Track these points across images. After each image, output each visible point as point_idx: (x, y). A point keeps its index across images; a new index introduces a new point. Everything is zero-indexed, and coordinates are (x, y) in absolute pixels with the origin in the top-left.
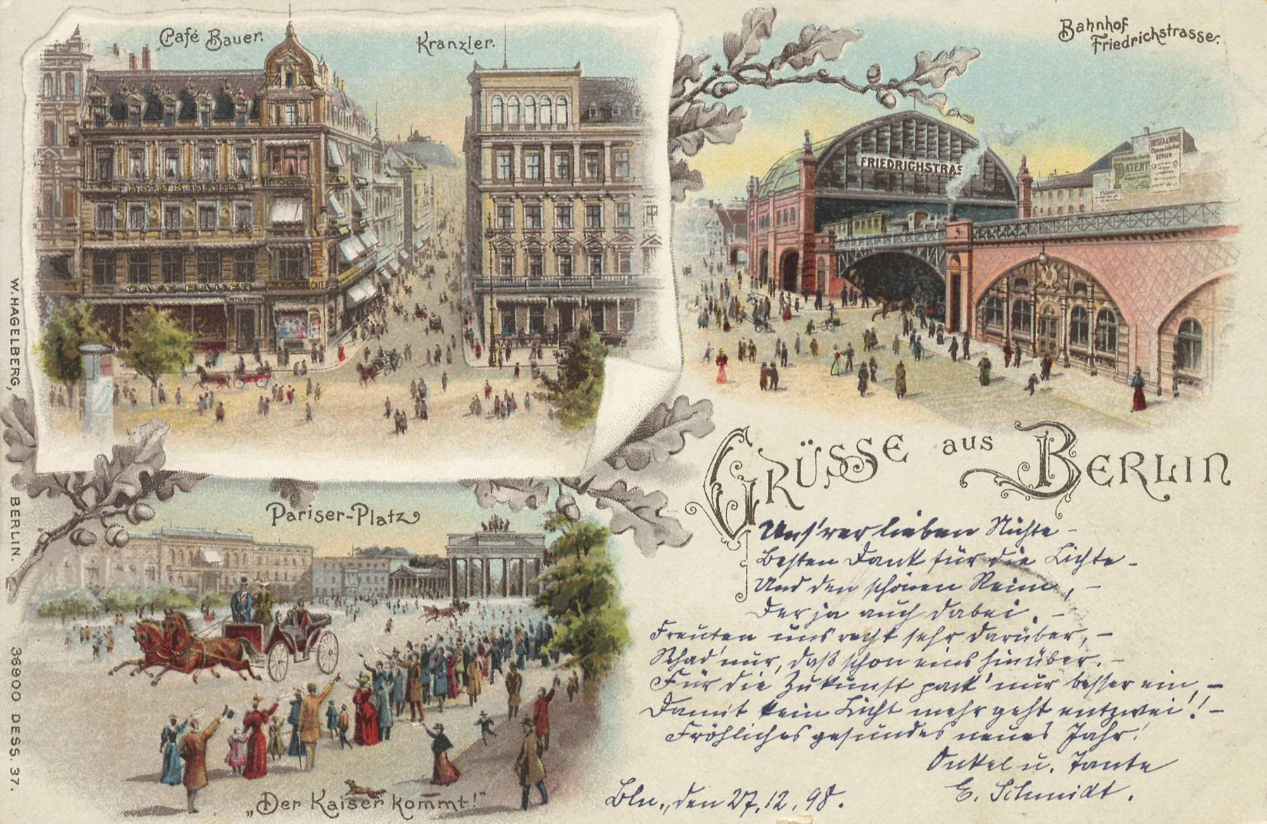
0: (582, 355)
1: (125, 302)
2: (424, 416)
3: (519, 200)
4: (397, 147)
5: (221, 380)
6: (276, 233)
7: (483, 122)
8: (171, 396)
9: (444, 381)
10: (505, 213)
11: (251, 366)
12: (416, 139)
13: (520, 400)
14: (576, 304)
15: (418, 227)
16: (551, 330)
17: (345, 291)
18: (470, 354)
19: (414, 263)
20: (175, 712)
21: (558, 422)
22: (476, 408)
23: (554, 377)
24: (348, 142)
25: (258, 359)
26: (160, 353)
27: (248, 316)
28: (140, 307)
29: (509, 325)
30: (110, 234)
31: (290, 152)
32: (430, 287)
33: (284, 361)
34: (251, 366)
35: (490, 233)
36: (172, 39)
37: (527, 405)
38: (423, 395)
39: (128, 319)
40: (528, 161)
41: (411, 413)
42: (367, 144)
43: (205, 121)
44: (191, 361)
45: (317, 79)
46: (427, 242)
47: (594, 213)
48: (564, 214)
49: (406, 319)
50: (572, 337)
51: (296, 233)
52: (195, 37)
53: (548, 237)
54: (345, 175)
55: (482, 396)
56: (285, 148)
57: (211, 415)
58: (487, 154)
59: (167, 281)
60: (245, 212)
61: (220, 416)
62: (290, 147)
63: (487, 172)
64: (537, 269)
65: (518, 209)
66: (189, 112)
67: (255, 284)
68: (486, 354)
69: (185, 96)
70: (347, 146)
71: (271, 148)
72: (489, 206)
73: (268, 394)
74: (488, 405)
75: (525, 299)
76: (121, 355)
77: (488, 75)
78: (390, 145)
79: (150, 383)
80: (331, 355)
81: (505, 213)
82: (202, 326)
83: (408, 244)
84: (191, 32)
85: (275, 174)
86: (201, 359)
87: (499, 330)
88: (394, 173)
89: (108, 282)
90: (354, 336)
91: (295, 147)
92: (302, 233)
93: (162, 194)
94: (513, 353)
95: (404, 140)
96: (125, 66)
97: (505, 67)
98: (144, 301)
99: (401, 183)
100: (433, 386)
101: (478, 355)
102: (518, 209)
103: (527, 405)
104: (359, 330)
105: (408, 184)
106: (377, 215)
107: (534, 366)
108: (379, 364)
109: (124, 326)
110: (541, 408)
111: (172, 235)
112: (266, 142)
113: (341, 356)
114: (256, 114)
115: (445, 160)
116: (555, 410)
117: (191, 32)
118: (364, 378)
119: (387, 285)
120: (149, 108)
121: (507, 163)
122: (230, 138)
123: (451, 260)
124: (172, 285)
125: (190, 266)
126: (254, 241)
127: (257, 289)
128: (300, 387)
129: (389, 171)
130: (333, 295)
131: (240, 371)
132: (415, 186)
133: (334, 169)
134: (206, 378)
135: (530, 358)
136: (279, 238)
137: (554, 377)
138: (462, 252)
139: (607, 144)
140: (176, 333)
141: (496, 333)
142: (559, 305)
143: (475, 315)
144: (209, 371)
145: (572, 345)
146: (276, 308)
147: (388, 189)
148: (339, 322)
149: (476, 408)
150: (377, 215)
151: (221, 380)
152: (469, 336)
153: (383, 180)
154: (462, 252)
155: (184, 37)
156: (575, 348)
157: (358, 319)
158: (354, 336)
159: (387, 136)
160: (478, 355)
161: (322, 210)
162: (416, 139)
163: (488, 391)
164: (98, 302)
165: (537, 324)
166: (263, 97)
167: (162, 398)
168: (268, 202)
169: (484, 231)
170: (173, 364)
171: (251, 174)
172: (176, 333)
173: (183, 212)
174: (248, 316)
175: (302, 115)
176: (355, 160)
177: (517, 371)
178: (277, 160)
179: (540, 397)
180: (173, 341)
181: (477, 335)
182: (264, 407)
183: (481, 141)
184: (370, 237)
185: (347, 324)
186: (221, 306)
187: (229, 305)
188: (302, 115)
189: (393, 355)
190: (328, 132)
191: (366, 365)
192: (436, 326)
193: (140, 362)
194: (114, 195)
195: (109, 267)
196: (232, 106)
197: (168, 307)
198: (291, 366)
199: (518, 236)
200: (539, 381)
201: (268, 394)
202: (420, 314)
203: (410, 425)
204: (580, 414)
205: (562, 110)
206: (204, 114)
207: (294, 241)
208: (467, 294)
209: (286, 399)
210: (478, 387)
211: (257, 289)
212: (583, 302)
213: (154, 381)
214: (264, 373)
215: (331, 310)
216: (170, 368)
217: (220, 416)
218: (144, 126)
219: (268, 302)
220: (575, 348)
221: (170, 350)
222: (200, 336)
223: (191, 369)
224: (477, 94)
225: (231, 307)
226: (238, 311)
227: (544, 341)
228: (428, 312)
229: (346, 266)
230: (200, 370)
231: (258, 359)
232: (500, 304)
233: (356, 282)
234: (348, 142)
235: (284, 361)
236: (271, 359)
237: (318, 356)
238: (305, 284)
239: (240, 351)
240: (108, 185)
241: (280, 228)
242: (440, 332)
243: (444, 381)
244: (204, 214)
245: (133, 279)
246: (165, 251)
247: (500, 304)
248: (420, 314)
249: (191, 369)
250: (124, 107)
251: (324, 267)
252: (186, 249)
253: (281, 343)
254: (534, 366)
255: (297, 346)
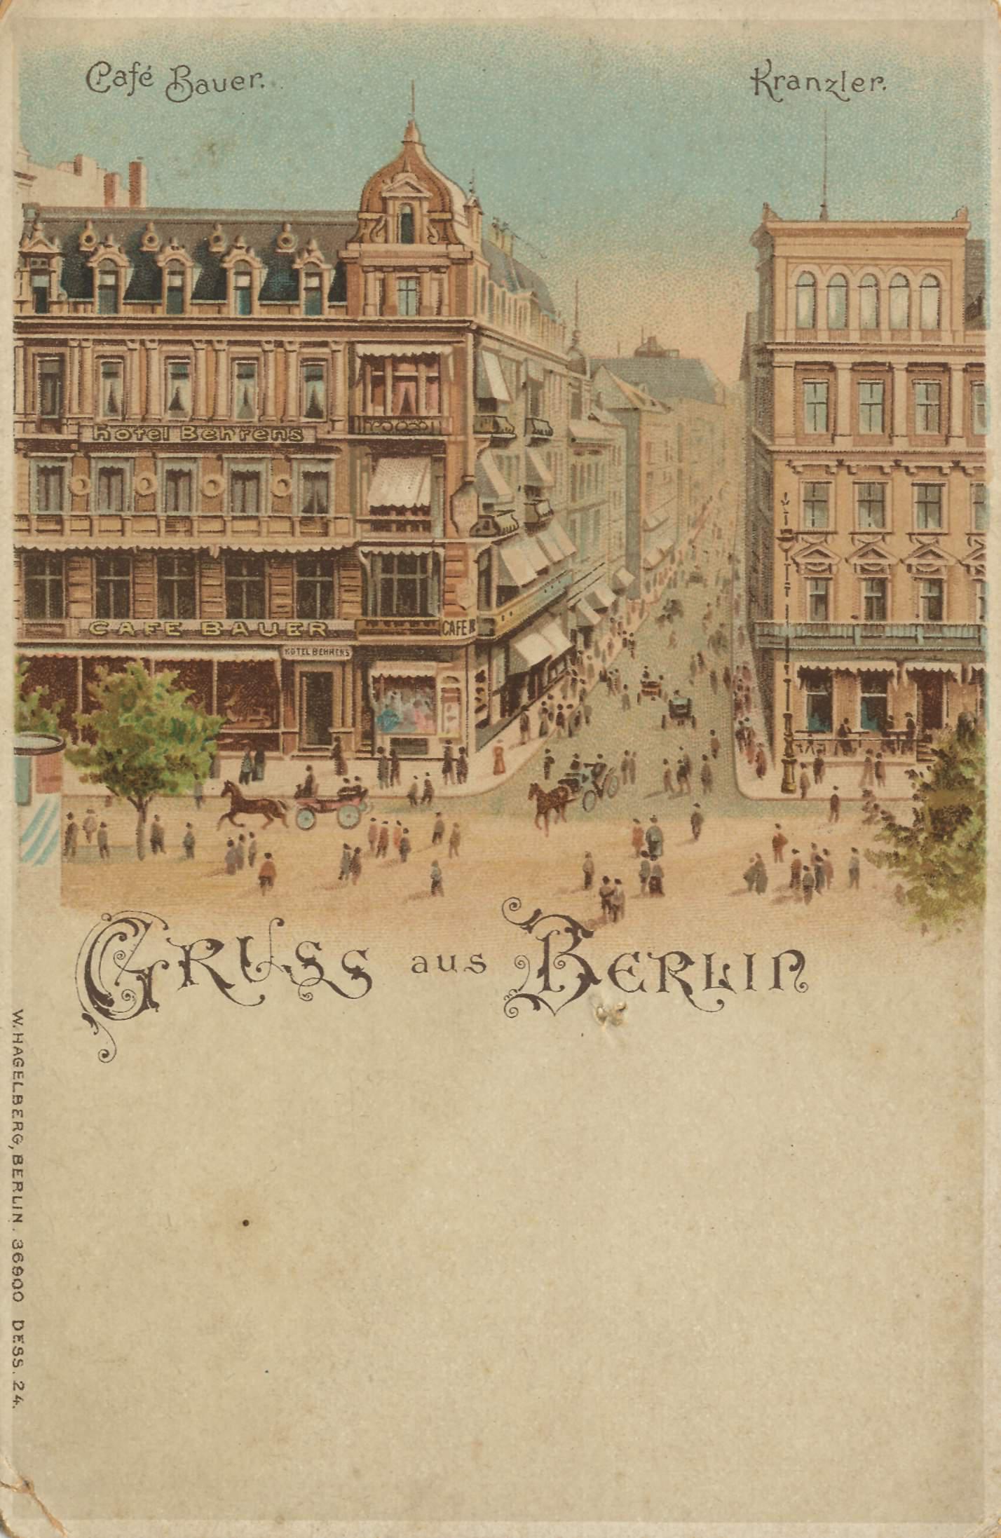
0: (960, 775)
1: (89, 653)
2: (656, 888)
3: (844, 472)
4: (616, 365)
5: (271, 809)
6: (378, 526)
7: (779, 323)
8: (174, 838)
9: (696, 821)
10: (816, 500)
11: (329, 786)
12: (651, 353)
13: (840, 863)
14: (949, 676)
15: (652, 523)
16: (901, 727)
17: (505, 642)
18: (745, 768)
19: (643, 591)
20: (766, 201)
21: (911, 909)
22: (756, 878)
23: (906, 819)
24: (522, 356)
25: (341, 769)
26: (155, 756)
27: (320, 684)
28: (117, 665)
29: (821, 711)
30: (59, 520)
31: (406, 370)
32: (672, 641)
33: (388, 772)
34: (329, 786)
35: (789, 536)
36: (107, 81)
37: (854, 873)
38: (654, 845)
39: (91, 686)
40: (864, 394)
41: (631, 885)
42: (558, 360)
43: (247, 307)
44: (213, 773)
45: (461, 232)
46: (667, 554)
47: (931, 503)
48: (873, 502)
49: (626, 701)
50: (943, 737)
51: (415, 526)
52: (145, 78)
53: (898, 548)
54: (514, 414)
55: (767, 851)
56: (396, 361)
57: (249, 875)
58: (785, 382)
59: (166, 614)
60: (320, 486)
61: (266, 880)
62: (404, 359)
63: (784, 422)
64: (877, 607)
65: (843, 492)
66: (214, 287)
67: (334, 624)
68: (775, 774)
69: (203, 253)
70: (519, 363)
71: (367, 359)
72: (788, 483)
73: (359, 838)
74: (778, 874)
75: (853, 667)
76: (82, 759)
77: (791, 234)
78: (602, 364)
79: (135, 814)
80: (479, 763)
81: (816, 500)
82: (231, 702)
83: (633, 558)
84: (141, 70)
85: (374, 410)
86: (231, 767)
87: (802, 721)
88: (603, 415)
89: (53, 617)
90: (525, 727)
91: (415, 360)
92: (428, 526)
93: (154, 447)
94: (828, 772)
95: (628, 352)
96: (96, 199)
97: (824, 217)
98: (124, 653)
99: (620, 437)
100: (675, 831)
101: (761, 772)
102: (843, 492)
103: (854, 873)
104: (534, 713)
105: (634, 445)
106: (574, 499)
107: (867, 793)
108: (572, 783)
109: (86, 700)
110: (880, 878)
111: (180, 527)
112: (361, 350)
113: (498, 770)
114: (339, 292)
115: (708, 394)
116: (907, 886)
117: (141, 70)
118: (542, 811)
119: (587, 630)
120: (136, 276)
121: (821, 396)
122: (294, 340)
123: (714, 588)
124: (176, 622)
125: (213, 584)
126: (334, 543)
127: (338, 634)
128: (420, 825)
129: (597, 412)
130: (484, 648)
131: (306, 791)
132: (649, 445)
133: (488, 404)
134: (241, 805)
135: (862, 783)
136: (384, 536)
137: (906, 819)
138: (736, 576)
139: (383, 576)
140: (185, 715)
141: (794, 727)
142: (916, 676)
143: (756, 697)
144: (250, 791)
145: (941, 754)
146: (374, 673)
147: (596, 449)
148: (497, 699)
149: (756, 878)
150: (574, 499)
151: (271, 809)
152: (743, 736)
153: (583, 429)
154: (736, 576)
155: (129, 77)
156: (948, 759)
157: (532, 697)
158: (525, 727)
159: (596, 346)
160: (761, 772)
161: (465, 485)
162: (651, 353)
163: (778, 843)
164: (40, 653)
165: (876, 713)
166: (354, 261)
167: (157, 843)
168: (364, 469)
169: (778, 534)
170: (178, 777)
171: (331, 407)
172: (185, 715)
173: (201, 480)
174: (320, 684)
175: (431, 298)
176: (531, 389)
177: (835, 803)
178: (379, 382)
179: (878, 859)
180: (179, 732)
181: (761, 738)
182: (352, 865)
183: (772, 352)
184: (556, 540)
185: (511, 707)
186: (270, 664)
187: (284, 661)
188: (431, 298)
189: (598, 770)
190: (479, 332)
191: (548, 786)
192: (681, 714)
193: (115, 770)
194: (65, 445)
195: (57, 585)
196: (295, 275)
197: (171, 665)
198: (402, 789)
199: (840, 547)
200: (879, 827)
201: (359, 838)
202: (651, 688)
203: (629, 905)
204: (954, 895)
205: (930, 297)
206: (246, 291)
207: (414, 544)
208: (744, 655)
209: (393, 851)
210: (758, 831)
211: (338, 634)
212: (964, 671)
213: (141, 808)
214: (355, 794)
215: (480, 678)
216: (174, 786)
217: (266, 880)
218: (126, 311)
219: (364, 658)
220: (948, 759)
221: (177, 750)
222: (228, 722)
223: (212, 787)
224: (767, 271)
225: (288, 666)
226: (302, 675)
227: (889, 746)
228: (668, 689)
229: (509, 593)
230: (229, 788)
231: (341, 769)
232: (804, 674)
233: (529, 624)
234: (522, 356)
235: (388, 772)
236: (364, 771)
237: (455, 766)
238: (434, 628)
239: (305, 753)
240: (58, 426)
241: (383, 518)
242: (688, 723)
243: (696, 821)
244: (239, 486)
245: (102, 611)
246: (164, 559)
247: (804, 674)
248: (651, 688)
249: (212, 787)
250: (88, 274)
251: (467, 591)
252: (204, 552)
253: (383, 741)
254: (867, 793)
255: (417, 746)
